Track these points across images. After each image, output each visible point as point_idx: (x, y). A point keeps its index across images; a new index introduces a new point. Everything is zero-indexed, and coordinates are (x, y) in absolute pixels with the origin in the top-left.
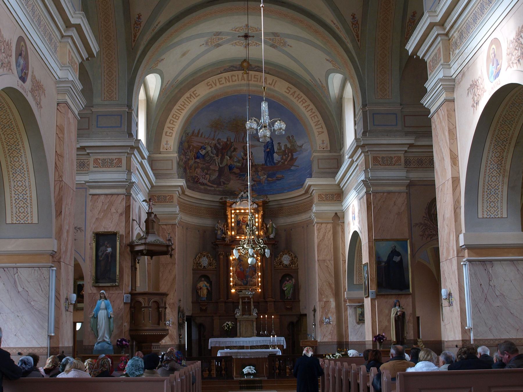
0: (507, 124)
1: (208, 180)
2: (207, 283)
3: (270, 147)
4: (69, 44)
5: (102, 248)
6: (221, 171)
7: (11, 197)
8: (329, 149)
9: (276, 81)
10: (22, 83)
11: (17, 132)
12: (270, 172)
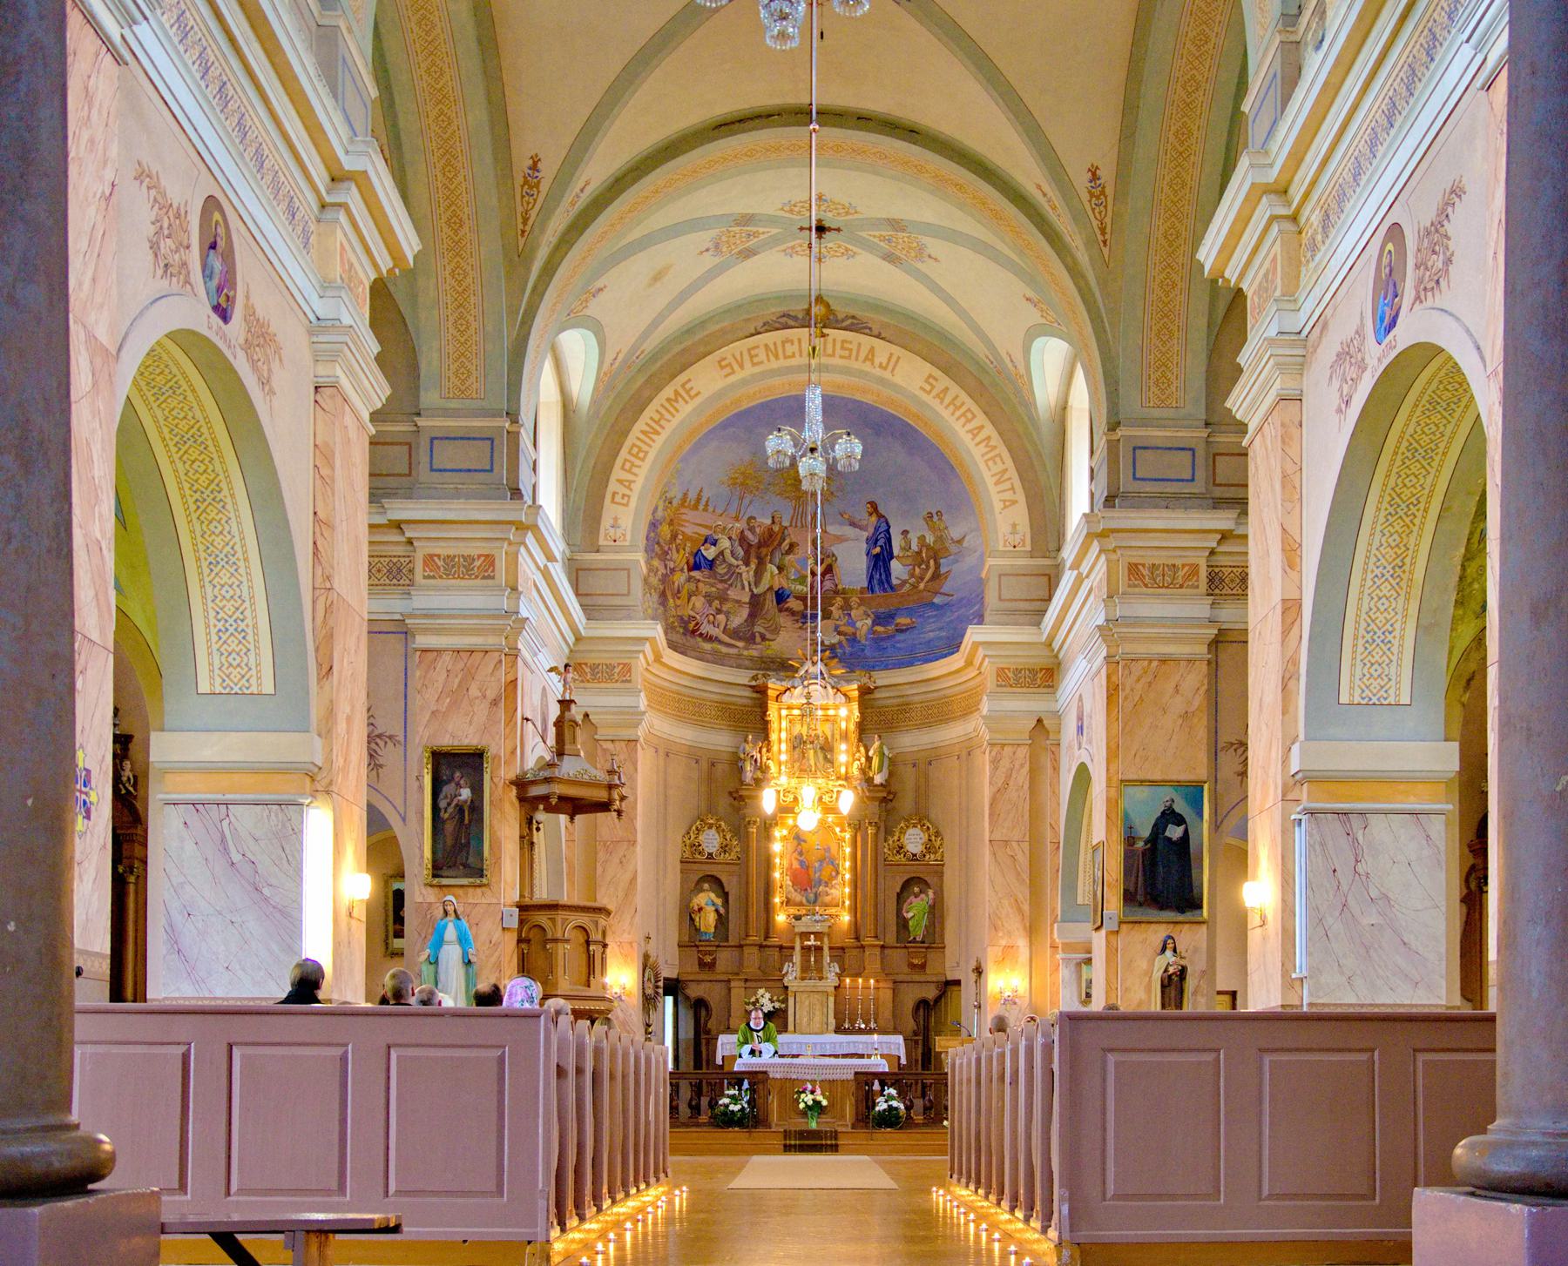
0: (1418, 457)
1: (722, 627)
2: (718, 896)
3: (881, 542)
4: (342, 228)
5: (448, 790)
6: (756, 603)
7: (207, 626)
8: (1028, 548)
9: (899, 358)
10: (221, 322)
11: (215, 456)
12: (882, 610)
